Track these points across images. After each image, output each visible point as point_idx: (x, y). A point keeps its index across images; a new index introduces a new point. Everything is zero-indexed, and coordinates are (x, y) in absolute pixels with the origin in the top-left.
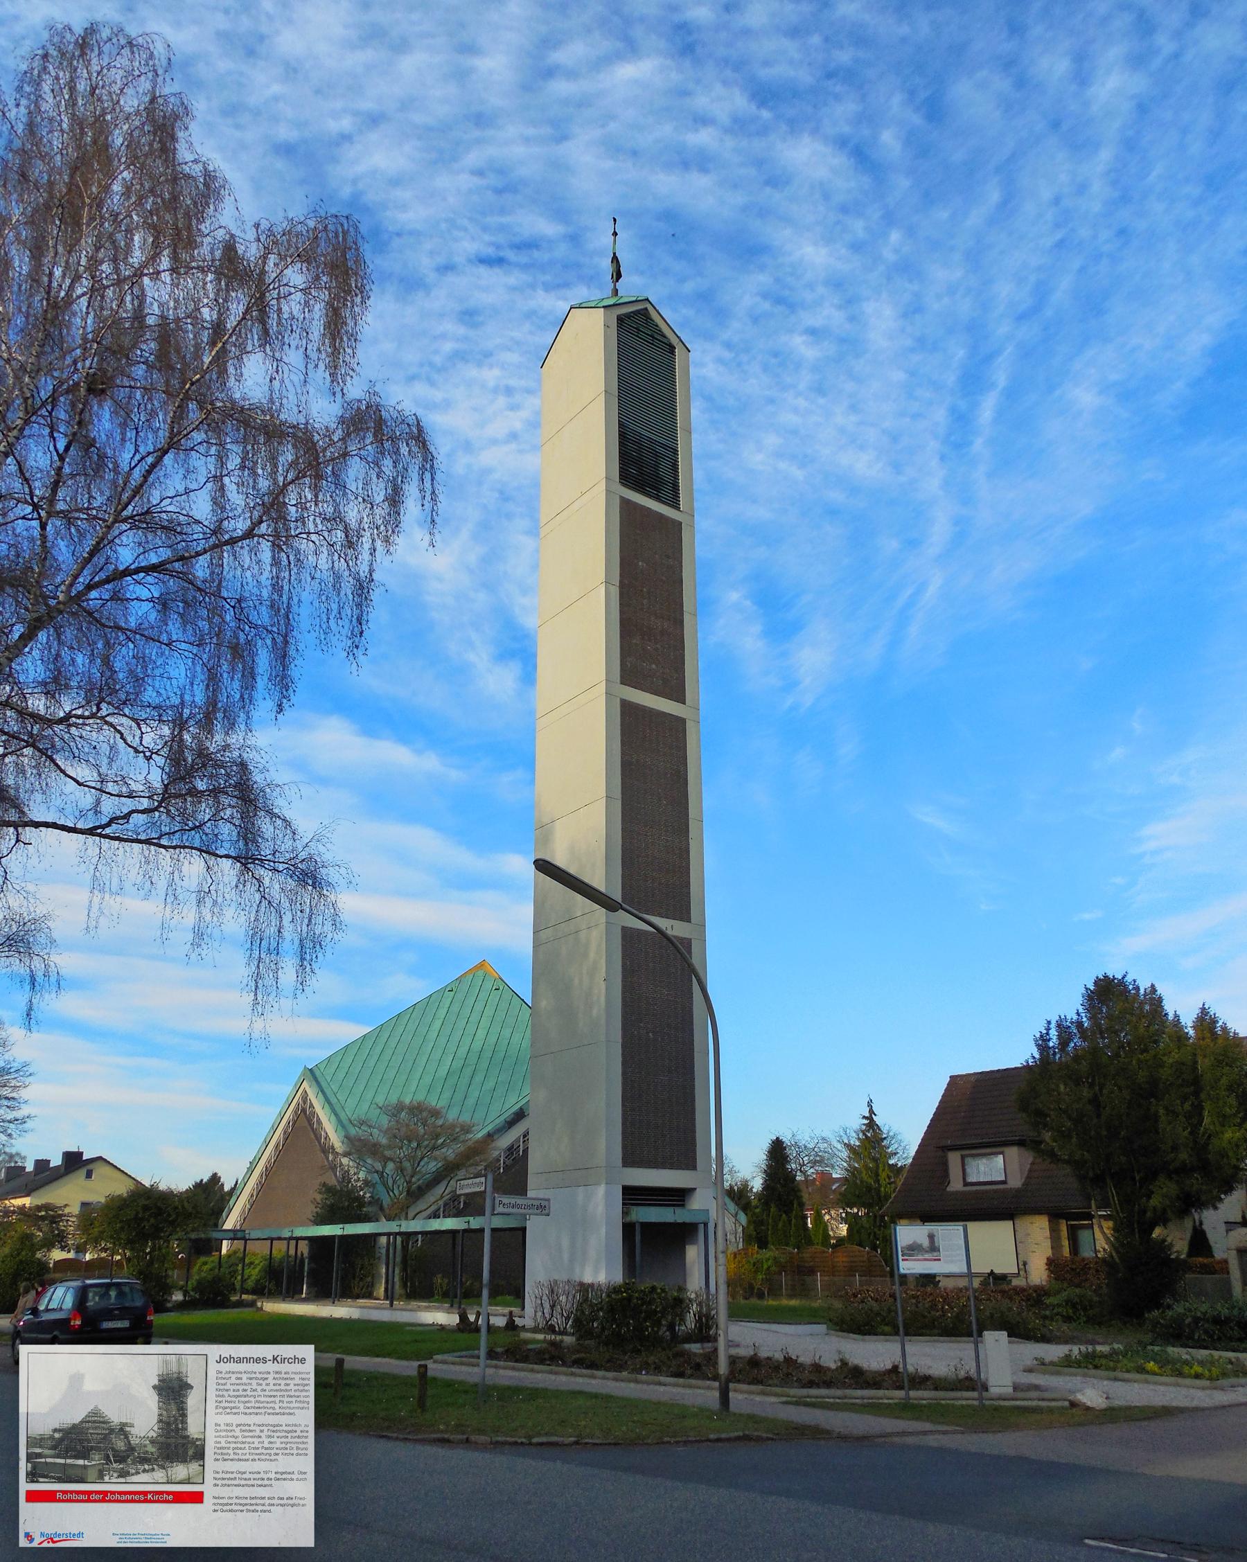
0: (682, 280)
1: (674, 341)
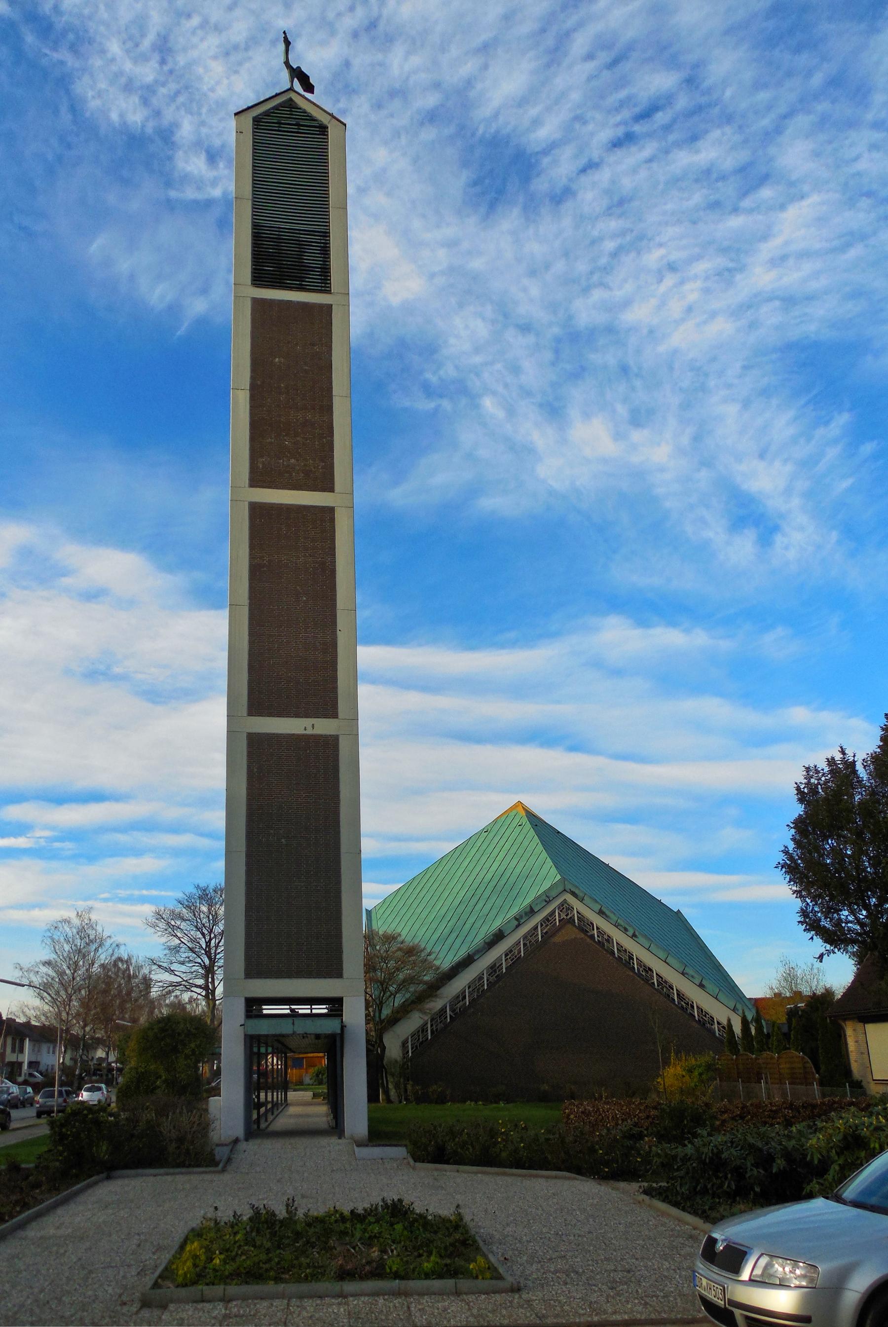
0: (809, 74)
1: (324, 119)
